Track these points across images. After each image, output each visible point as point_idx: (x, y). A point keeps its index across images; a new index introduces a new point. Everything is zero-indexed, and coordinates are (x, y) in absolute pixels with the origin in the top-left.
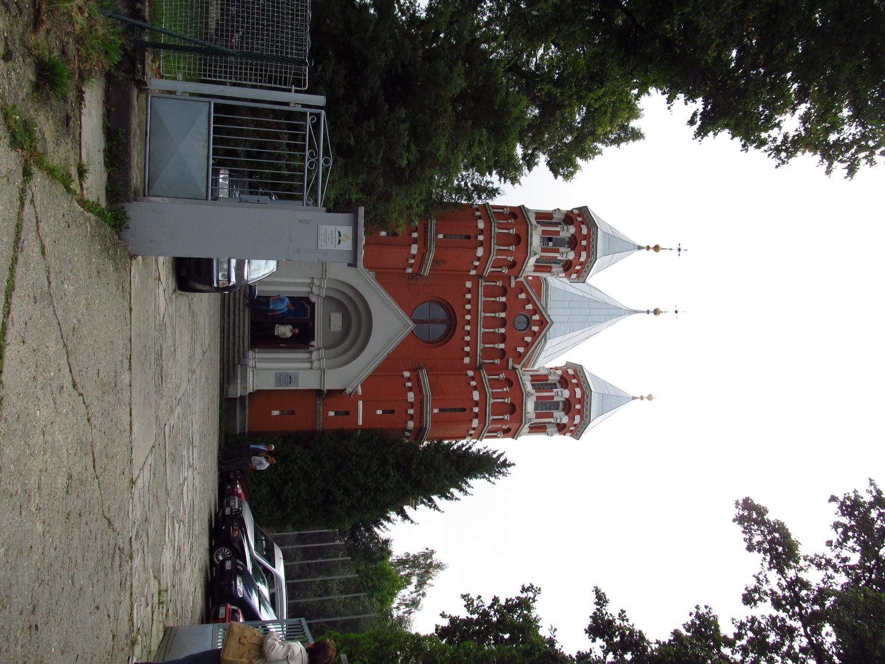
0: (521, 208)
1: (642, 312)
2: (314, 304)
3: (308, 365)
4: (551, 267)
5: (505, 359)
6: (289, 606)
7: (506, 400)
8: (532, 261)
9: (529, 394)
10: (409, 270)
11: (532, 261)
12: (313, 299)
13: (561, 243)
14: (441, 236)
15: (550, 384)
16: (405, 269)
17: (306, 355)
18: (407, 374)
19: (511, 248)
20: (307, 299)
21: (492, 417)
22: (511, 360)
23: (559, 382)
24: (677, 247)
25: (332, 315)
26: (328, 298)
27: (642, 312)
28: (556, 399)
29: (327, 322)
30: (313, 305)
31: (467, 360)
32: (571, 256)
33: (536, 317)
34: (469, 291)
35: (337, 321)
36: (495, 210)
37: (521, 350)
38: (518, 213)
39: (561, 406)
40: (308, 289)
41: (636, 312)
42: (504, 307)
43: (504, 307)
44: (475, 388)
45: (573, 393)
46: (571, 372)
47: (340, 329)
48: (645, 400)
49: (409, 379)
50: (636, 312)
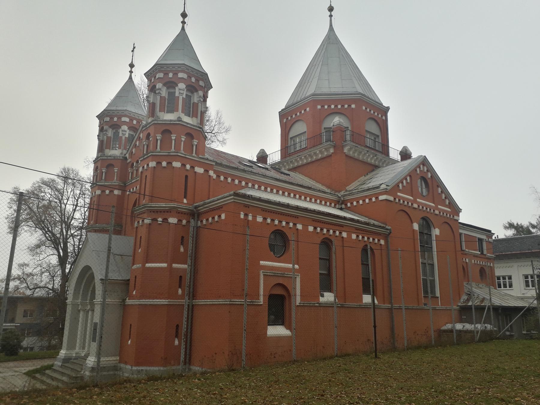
1: (331, 20)
3: (90, 313)
4: (194, 103)
6: (9, 323)
7: (183, 139)
8: (187, 119)
9: (179, 119)
11: (187, 119)
13: (172, 95)
14: (185, 201)
19: (173, 138)
21: (194, 154)
27: (331, 20)
28: (184, 96)
32: (182, 86)
41: (331, 25)
44: (377, 198)
45: (182, 80)
48: (186, 20)
50: (331, 25)
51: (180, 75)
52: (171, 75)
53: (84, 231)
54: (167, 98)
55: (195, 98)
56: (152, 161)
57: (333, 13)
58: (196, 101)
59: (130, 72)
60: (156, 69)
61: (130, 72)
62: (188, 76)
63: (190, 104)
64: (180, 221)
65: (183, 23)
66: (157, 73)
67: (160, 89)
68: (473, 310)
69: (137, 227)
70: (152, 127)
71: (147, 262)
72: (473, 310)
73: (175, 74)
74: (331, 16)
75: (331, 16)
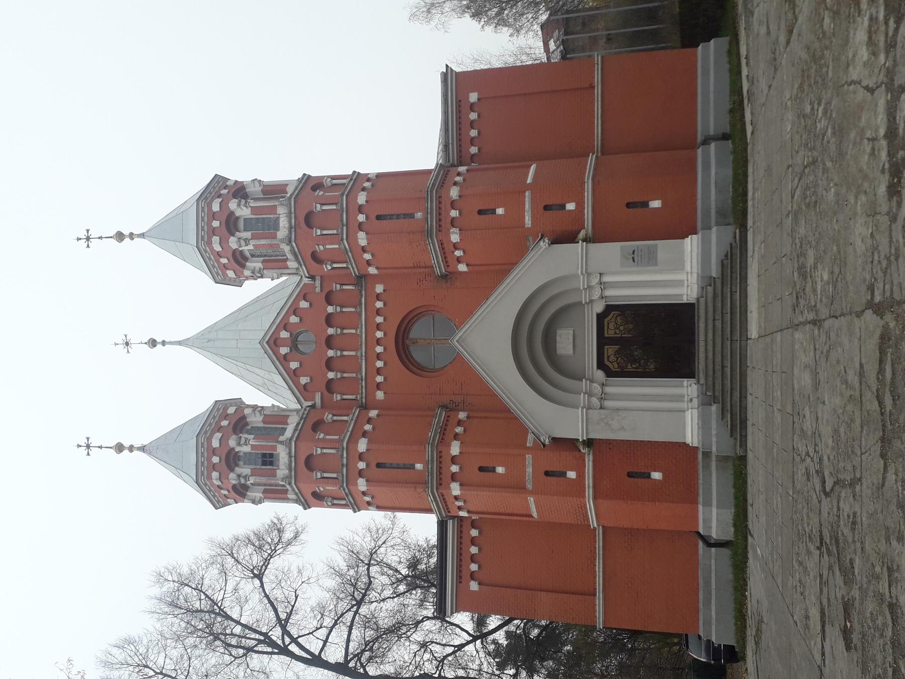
0: (307, 506)
1: (171, 343)
2: (599, 367)
4: (264, 422)
5: (326, 291)
10: (462, 415)
12: (600, 375)
15: (259, 256)
16: (468, 417)
17: (608, 293)
18: (462, 268)
20: (610, 374)
22: (318, 290)
23: (246, 259)
24: (93, 451)
25: (571, 352)
26: (578, 377)
27: (171, 343)
29: (579, 342)
30: (601, 365)
31: (379, 289)
33: (284, 350)
34: (378, 386)
35: (564, 343)
36: (343, 502)
37: (304, 304)
38: (311, 499)
39: (241, 224)
40: (608, 389)
41: (179, 343)
42: (329, 364)
43: (329, 364)
46: (231, 274)
47: (559, 332)
49: (459, 260)
50: (179, 343)
51: (215, 443)
52: (215, 460)
53: (478, 642)
54: (253, 467)
55: (256, 420)
56: (356, 484)
57: (159, 340)
58: (261, 418)
59: (132, 239)
60: (206, 485)
61: (132, 239)
62: (218, 431)
63: (265, 428)
64: (456, 437)
65: (131, 449)
66: (212, 484)
67: (239, 476)
68: (714, 458)
69: (469, 512)
70: (301, 485)
71: (524, 488)
72: (714, 458)
73: (214, 452)
74: (164, 343)
75: (164, 343)
